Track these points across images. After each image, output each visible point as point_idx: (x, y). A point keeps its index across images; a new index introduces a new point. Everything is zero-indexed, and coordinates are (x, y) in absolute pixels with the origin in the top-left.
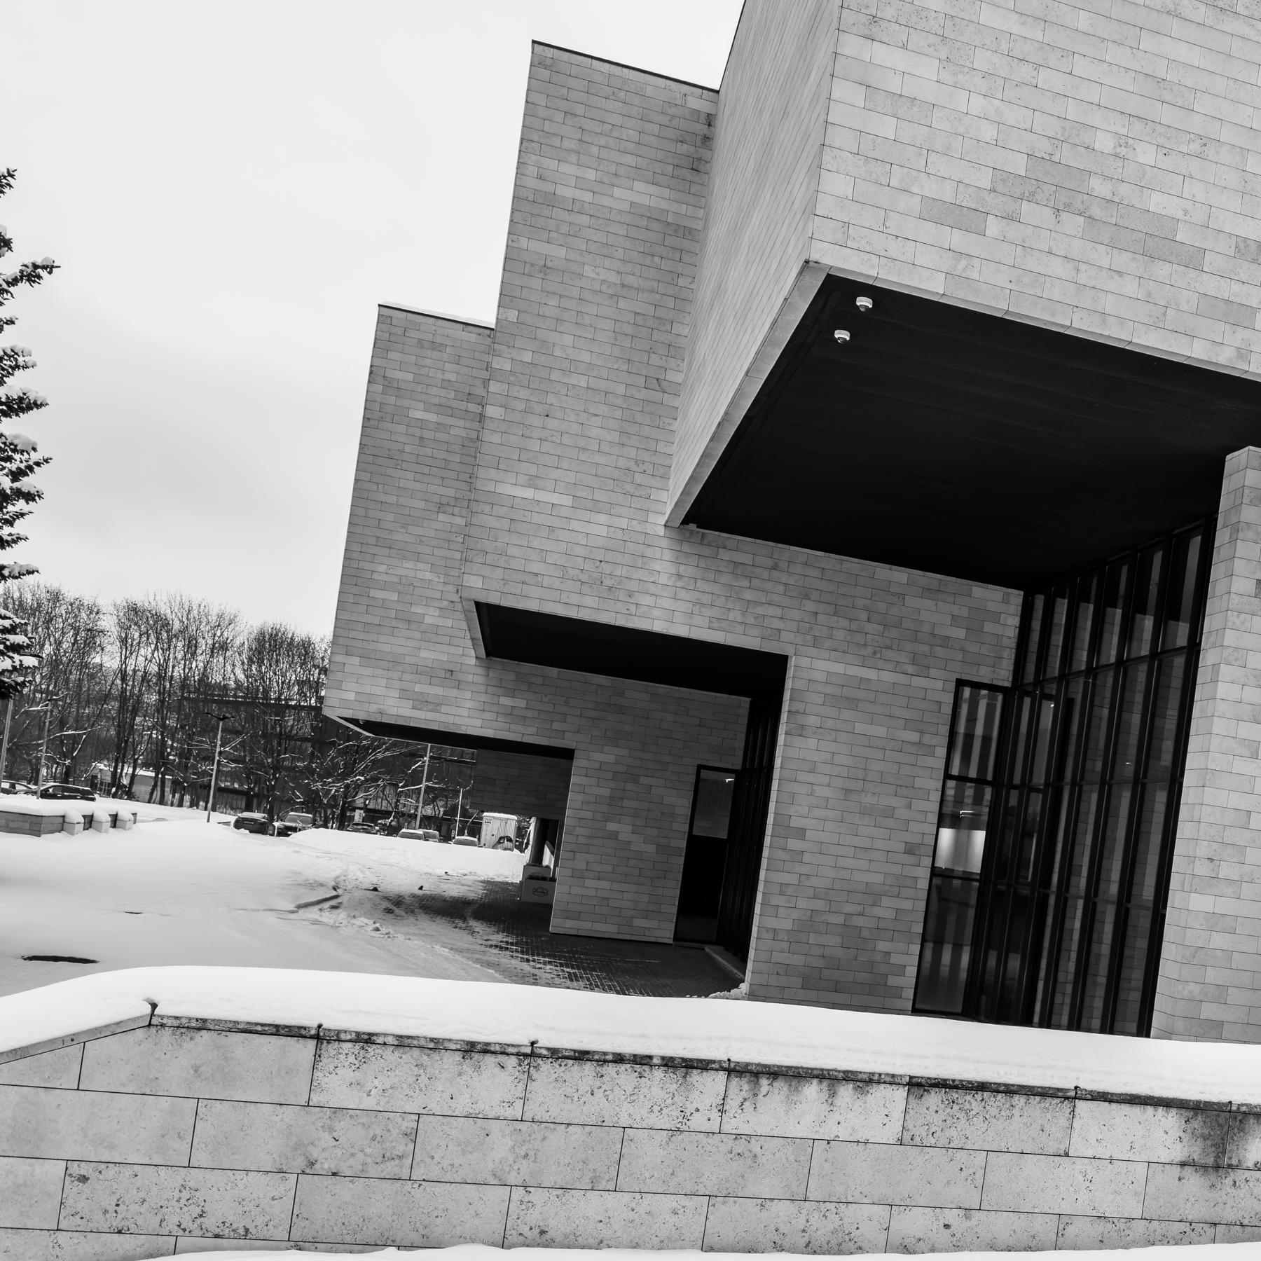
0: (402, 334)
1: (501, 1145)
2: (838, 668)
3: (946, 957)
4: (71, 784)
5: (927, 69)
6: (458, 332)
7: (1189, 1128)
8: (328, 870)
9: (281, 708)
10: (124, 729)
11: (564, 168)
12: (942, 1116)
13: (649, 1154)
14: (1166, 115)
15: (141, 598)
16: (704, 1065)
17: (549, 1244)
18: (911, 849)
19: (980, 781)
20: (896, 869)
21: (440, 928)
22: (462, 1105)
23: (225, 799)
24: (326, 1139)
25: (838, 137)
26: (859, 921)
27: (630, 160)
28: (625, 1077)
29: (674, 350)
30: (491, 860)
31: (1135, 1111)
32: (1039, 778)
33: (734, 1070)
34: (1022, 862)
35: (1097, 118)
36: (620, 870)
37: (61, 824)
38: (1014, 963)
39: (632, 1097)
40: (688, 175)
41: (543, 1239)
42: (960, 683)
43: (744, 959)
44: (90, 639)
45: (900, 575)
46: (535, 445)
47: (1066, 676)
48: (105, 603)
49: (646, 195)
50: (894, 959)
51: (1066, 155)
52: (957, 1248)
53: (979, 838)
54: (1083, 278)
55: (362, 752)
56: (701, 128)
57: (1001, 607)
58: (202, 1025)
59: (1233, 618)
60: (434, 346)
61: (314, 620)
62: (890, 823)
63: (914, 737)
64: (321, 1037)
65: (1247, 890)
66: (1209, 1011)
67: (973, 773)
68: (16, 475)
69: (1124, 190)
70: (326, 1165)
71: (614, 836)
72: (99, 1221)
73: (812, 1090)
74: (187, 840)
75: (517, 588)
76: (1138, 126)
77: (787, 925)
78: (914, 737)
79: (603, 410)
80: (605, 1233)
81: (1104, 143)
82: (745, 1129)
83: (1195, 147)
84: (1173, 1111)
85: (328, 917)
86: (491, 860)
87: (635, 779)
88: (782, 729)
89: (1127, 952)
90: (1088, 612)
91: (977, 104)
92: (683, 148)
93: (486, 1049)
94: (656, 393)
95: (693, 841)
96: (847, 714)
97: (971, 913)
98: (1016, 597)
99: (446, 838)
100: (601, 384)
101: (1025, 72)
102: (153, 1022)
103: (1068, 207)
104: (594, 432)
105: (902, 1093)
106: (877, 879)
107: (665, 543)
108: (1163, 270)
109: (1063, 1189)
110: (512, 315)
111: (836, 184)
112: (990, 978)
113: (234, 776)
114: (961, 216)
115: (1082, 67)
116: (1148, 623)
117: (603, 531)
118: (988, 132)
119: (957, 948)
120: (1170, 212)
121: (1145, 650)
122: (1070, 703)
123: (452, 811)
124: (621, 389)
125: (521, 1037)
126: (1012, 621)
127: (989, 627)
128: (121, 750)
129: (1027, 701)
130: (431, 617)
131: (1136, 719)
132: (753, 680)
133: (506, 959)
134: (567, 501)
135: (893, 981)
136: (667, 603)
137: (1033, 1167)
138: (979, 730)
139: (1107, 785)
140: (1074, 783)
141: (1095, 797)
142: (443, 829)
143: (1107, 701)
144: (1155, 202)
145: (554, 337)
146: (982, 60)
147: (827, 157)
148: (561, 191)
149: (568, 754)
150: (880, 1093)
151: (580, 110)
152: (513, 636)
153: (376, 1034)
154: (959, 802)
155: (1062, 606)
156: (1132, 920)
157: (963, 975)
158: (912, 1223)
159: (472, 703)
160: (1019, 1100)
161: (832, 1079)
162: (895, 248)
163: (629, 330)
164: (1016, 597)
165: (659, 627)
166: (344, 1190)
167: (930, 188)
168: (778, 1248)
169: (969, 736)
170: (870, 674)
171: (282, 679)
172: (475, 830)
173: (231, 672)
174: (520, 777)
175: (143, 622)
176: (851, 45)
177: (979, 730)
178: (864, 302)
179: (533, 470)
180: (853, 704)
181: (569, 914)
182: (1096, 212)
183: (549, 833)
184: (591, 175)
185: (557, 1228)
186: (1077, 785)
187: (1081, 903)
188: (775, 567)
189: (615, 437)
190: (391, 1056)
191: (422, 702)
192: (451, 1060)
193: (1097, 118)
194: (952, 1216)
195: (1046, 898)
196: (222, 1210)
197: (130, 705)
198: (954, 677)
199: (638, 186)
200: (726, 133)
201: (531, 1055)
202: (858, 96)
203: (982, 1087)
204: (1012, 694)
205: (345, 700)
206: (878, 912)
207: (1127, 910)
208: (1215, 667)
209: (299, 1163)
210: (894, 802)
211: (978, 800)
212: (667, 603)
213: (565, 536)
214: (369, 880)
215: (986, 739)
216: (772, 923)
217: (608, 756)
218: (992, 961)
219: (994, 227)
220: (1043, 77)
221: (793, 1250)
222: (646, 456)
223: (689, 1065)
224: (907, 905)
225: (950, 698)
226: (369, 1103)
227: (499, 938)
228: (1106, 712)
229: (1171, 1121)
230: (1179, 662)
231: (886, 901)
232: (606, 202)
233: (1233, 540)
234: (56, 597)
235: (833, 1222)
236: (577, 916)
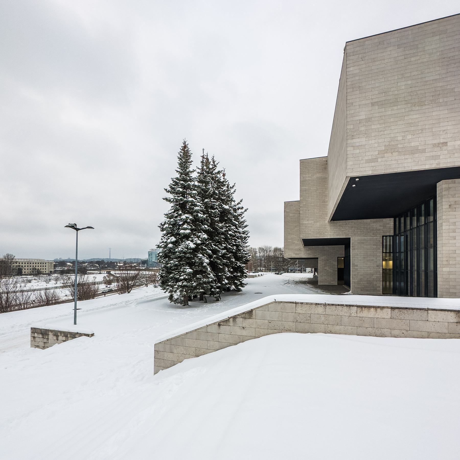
0: (287, 205)
1: (323, 318)
2: (360, 238)
3: (388, 283)
4: (256, 271)
6: (295, 202)
7: (457, 315)
8: (287, 279)
9: (278, 258)
10: (261, 263)
12: (399, 314)
13: (346, 319)
14: (412, 129)
15: (260, 247)
16: (353, 306)
17: (332, 333)
18: (378, 266)
19: (390, 252)
20: (376, 270)
21: (303, 285)
22: (316, 312)
23: (273, 271)
24: (299, 317)
26: (369, 279)
28: (340, 308)
29: (326, 196)
30: (308, 275)
31: (443, 312)
32: (403, 249)
33: (358, 306)
34: (401, 265)
36: (328, 275)
37: (256, 276)
38: (402, 284)
39: (342, 311)
41: (331, 332)
42: (383, 236)
43: (350, 287)
44: (256, 253)
45: (369, 221)
47: (405, 231)
48: (257, 248)
49: (318, 175)
50: (377, 285)
51: (392, 143)
52: (406, 337)
53: (391, 262)
54: (399, 162)
55: (289, 262)
57: (390, 222)
58: (281, 302)
59: (444, 213)
60: (292, 205)
61: (281, 245)
62: (373, 262)
63: (376, 247)
64: (296, 303)
65: (457, 266)
66: (451, 291)
67: (388, 251)
68: (247, 235)
69: (405, 145)
70: (299, 321)
71: (326, 270)
72: (272, 328)
73: (372, 309)
74: (270, 276)
76: (407, 133)
77: (357, 281)
78: (376, 247)
80: (341, 332)
81: (400, 138)
82: (361, 316)
83: (420, 131)
84: (452, 312)
85: (288, 285)
86: (308, 275)
87: (328, 260)
88: (351, 249)
89: (429, 280)
90: (408, 219)
93: (319, 304)
94: (324, 203)
95: (338, 268)
96: (362, 245)
97: (392, 276)
98: (392, 219)
99: (301, 272)
101: (382, 133)
102: (275, 302)
103: (394, 152)
105: (390, 310)
109: (428, 327)
110: (302, 198)
111: (350, 163)
112: (398, 287)
113: (274, 267)
116: (423, 218)
119: (390, 282)
120: (416, 145)
121: (423, 223)
122: (407, 236)
123: (302, 269)
125: (323, 302)
126: (392, 224)
128: (261, 266)
129: (398, 237)
130: (296, 242)
131: (423, 236)
132: (345, 243)
133: (313, 289)
136: (330, 233)
137: (420, 323)
138: (388, 244)
139: (418, 250)
140: (410, 250)
141: (416, 252)
142: (301, 271)
143: (416, 234)
144: (413, 144)
146: (373, 134)
147: (348, 160)
149: (317, 258)
150: (385, 310)
152: (308, 243)
154: (386, 256)
155: (402, 219)
156: (429, 274)
157: (392, 287)
158: (396, 332)
159: (303, 253)
160: (415, 311)
161: (376, 308)
162: (362, 169)
164: (392, 219)
166: (302, 324)
167: (366, 158)
168: (370, 335)
169: (386, 245)
170: (366, 238)
171: (278, 254)
172: (305, 271)
173: (272, 254)
174: (311, 263)
175: (261, 249)
177: (388, 244)
178: (357, 179)
180: (363, 243)
181: (321, 282)
182: (400, 150)
183: (316, 270)
185: (333, 331)
186: (411, 251)
187: (416, 272)
190: (306, 306)
191: (296, 254)
192: (314, 306)
193: (398, 135)
194: (404, 331)
195: (407, 272)
196: (287, 327)
197: (261, 260)
200: (329, 162)
201: (325, 305)
202: (352, 148)
203: (406, 308)
204: (394, 237)
205: (286, 256)
206: (373, 277)
207: (427, 273)
208: (442, 224)
209: (296, 321)
210: (373, 258)
211: (390, 256)
212: (330, 233)
214: (292, 279)
215: (390, 245)
216: (354, 281)
217: (323, 258)
218: (398, 284)
219: (379, 160)
220: (385, 132)
221: (373, 336)
223: (350, 306)
224: (379, 276)
226: (303, 312)
227: (311, 286)
228: (416, 236)
229: (452, 314)
230: (432, 224)
233: (442, 199)
234: (252, 248)
235: (380, 332)
236: (322, 282)
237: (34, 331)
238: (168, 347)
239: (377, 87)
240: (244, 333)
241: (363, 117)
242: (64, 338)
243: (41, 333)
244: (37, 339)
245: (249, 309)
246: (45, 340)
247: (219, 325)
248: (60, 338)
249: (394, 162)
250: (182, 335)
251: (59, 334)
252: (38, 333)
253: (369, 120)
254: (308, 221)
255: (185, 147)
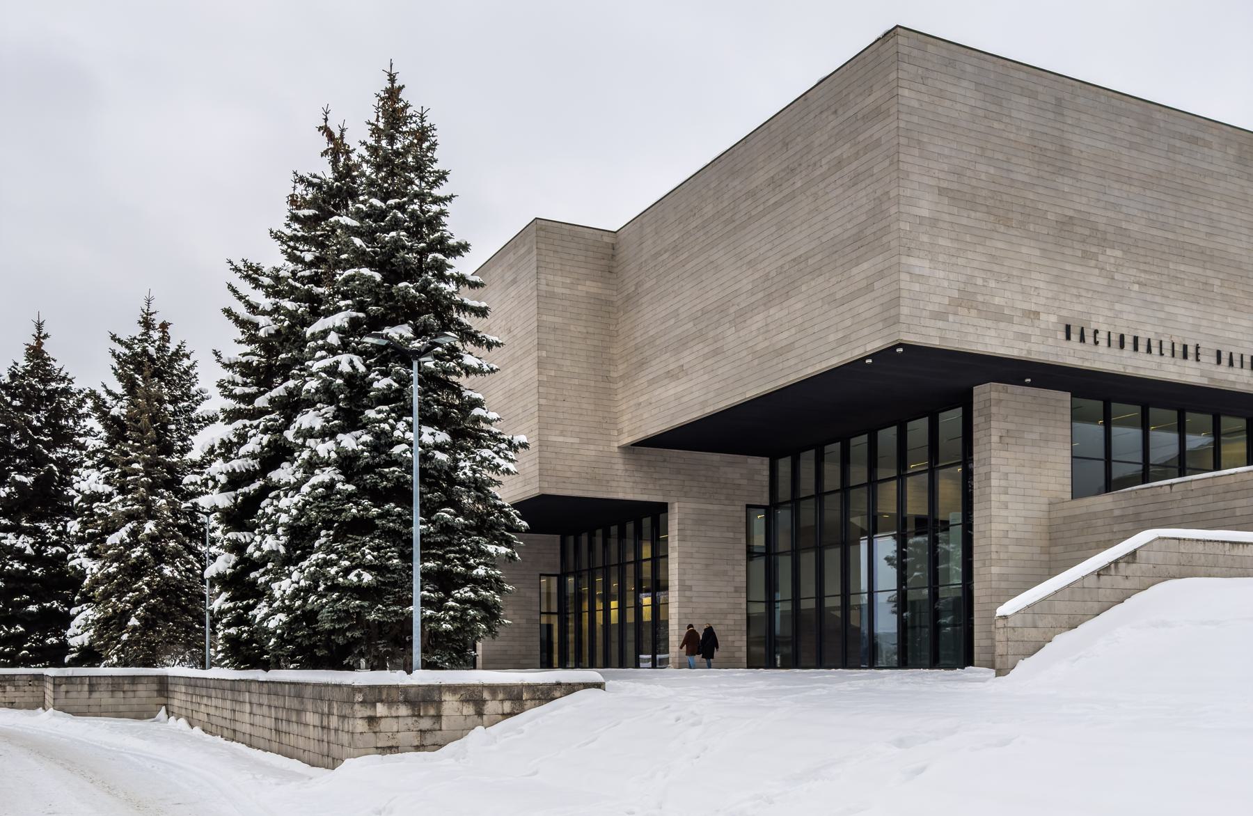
5: (926, 264)
11: (557, 278)
14: (996, 268)
20: (732, 601)
25: (904, 294)
27: (583, 271)
33: (1231, 543)
35: (976, 273)
40: (607, 275)
45: (716, 457)
46: (560, 415)
49: (591, 287)
50: (737, 644)
51: (969, 288)
56: (610, 251)
57: (760, 465)
69: (987, 298)
75: (561, 485)
78: (731, 535)
79: (587, 395)
81: (980, 282)
91: (942, 274)
92: (603, 262)
98: (766, 460)
100: (584, 382)
104: (585, 406)
106: (725, 606)
107: (618, 455)
108: (1002, 325)
114: (940, 316)
115: (970, 255)
117: (593, 453)
118: (946, 284)
124: (592, 384)
127: (756, 477)
134: (577, 440)
135: (737, 655)
144: (997, 300)
145: (562, 362)
148: (556, 290)
151: (559, 249)
153: (506, 716)
163: (592, 354)
165: (621, 496)
167: (930, 307)
170: (710, 507)
176: (904, 259)
179: (561, 427)
184: (568, 281)
188: (665, 461)
189: (592, 407)
193: (976, 273)
198: (744, 504)
199: (588, 283)
206: (727, 622)
213: (578, 457)
219: (951, 318)
222: (606, 415)
225: (744, 514)
231: (729, 616)
232: (576, 293)
237: (370, 698)
238: (1029, 618)
239: (947, 157)
240: (1128, 584)
241: (925, 213)
242: (507, 707)
243: (407, 702)
244: (384, 725)
245: (1131, 549)
246: (426, 724)
247: (1099, 575)
248: (492, 707)
249: (971, 330)
250: (1049, 596)
251: (486, 695)
252: (390, 703)
253: (934, 222)
254: (562, 434)
255: (393, 94)
